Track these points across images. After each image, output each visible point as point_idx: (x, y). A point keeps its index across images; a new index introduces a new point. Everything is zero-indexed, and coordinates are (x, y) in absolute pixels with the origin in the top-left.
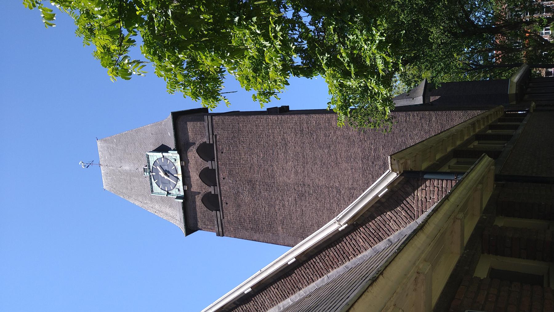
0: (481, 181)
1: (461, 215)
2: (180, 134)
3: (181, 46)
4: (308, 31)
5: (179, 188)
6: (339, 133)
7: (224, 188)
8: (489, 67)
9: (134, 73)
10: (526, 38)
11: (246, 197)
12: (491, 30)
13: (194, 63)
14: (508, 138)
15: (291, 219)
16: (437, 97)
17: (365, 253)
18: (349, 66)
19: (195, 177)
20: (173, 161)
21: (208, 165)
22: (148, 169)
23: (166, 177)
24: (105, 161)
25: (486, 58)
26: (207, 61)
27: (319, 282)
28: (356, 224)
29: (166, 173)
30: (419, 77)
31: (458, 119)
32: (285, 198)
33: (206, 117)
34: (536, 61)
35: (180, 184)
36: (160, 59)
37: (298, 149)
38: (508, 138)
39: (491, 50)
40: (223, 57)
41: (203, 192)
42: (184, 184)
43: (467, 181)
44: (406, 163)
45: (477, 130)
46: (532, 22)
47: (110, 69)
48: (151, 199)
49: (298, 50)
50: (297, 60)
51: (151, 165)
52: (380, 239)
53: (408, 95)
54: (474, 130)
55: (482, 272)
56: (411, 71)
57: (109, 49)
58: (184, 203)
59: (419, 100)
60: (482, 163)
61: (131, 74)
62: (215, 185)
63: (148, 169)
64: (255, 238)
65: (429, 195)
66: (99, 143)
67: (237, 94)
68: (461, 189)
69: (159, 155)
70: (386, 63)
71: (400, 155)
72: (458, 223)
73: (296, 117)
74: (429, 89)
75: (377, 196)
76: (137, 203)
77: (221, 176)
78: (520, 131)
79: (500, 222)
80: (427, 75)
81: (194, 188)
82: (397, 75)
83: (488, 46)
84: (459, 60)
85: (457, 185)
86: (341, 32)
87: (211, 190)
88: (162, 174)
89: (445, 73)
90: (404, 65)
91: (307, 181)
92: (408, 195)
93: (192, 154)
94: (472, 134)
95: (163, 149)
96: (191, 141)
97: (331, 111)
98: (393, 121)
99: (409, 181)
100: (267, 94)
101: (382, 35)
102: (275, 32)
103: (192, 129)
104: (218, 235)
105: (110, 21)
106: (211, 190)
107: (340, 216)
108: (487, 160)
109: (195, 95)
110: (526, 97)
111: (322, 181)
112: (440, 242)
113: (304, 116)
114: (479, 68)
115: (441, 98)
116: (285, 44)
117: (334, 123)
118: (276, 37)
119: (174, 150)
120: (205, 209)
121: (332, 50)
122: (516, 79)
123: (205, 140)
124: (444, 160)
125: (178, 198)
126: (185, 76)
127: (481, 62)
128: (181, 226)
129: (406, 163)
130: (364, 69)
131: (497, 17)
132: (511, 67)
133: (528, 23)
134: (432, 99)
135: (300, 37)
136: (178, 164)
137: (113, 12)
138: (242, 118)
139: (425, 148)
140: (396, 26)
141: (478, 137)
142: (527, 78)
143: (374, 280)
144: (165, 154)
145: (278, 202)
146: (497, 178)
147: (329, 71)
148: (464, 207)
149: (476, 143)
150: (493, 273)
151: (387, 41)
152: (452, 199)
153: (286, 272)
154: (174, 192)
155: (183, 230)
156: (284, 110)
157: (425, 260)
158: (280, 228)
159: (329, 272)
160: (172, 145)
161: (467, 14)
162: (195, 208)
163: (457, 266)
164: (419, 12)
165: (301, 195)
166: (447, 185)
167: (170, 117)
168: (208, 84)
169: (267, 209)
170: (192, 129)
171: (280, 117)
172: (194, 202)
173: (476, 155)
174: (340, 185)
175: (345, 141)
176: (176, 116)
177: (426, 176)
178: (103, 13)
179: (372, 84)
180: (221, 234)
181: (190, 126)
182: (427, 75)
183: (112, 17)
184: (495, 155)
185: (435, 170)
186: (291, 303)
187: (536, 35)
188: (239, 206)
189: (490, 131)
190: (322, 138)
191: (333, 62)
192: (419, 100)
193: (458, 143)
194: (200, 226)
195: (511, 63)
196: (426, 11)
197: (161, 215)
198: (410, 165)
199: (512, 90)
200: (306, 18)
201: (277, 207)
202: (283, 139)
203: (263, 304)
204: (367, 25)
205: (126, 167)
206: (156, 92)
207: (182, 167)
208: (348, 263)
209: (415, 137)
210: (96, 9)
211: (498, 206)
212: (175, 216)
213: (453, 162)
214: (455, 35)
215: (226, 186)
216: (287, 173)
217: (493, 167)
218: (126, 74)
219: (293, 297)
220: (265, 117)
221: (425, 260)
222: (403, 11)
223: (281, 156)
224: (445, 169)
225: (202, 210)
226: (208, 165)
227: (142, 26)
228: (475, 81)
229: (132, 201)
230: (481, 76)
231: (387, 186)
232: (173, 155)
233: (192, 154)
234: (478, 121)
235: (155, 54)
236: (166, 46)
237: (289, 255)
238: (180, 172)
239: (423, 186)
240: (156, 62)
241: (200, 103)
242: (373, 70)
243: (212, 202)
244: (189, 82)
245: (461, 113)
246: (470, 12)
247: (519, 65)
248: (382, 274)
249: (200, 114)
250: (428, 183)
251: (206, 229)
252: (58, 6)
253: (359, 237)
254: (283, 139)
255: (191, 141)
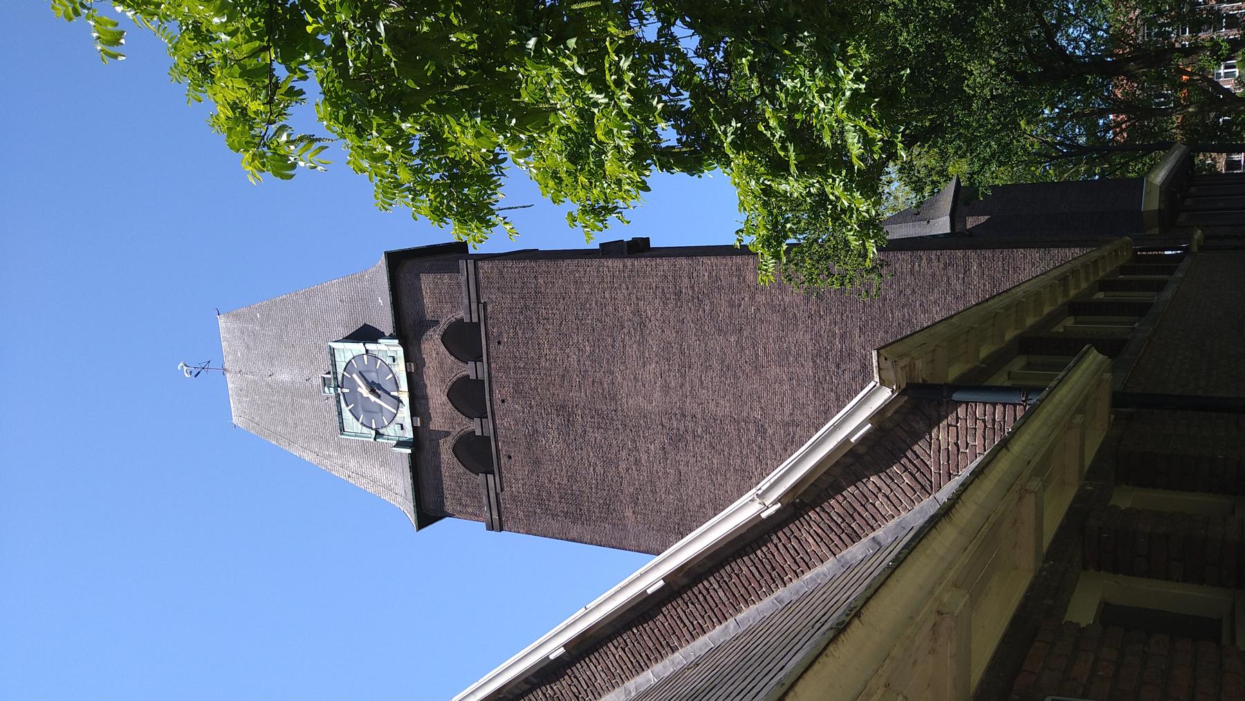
0: (1082, 406)
1: (1035, 484)
2: (405, 301)
3: (406, 104)
4: (691, 69)
5: (402, 423)
6: (761, 298)
7: (504, 423)
8: (1100, 149)
9: (301, 164)
10: (1182, 85)
11: (553, 444)
12: (1104, 67)
13: (435, 141)
14: (1141, 310)
15: (654, 492)
16: (983, 219)
17: (820, 569)
18: (784, 148)
19: (437, 397)
20: (389, 361)
21: (468, 370)
22: (334, 380)
23: (373, 398)
24: (236, 361)
25: (1091, 131)
26: (466, 137)
27: (717, 634)
28: (799, 503)
29: (374, 388)
30: (943, 173)
31: (1029, 267)
32: (641, 445)
33: (462, 263)
34: (1204, 137)
35: (405, 413)
36: (360, 132)
37: (670, 335)
38: (1141, 310)
39: (1103, 113)
40: (502, 128)
41: (457, 431)
42: (414, 413)
43: (1049, 407)
44: (911, 367)
45: (1072, 293)
46: (1195, 49)
47: (248, 156)
48: (340, 448)
49: (671, 113)
50: (668, 135)
51: (340, 370)
52: (855, 537)
53: (918, 213)
54: (1066, 292)
55: (1082, 610)
56: (924, 159)
57: (244, 111)
58: (412, 457)
59: (942, 225)
60: (1084, 366)
61: (294, 166)
62: (483, 416)
63: (334, 380)
64: (574, 534)
65: (964, 439)
66: (222, 321)
67: (532, 211)
68: (1036, 424)
69: (358, 348)
70: (867, 142)
71: (899, 348)
72: (1030, 501)
73: (665, 264)
74: (964, 200)
75: (846, 440)
76: (308, 457)
77: (497, 396)
78: (1168, 294)
79: (1124, 499)
80: (959, 168)
81: (437, 423)
82: (892, 168)
83: (1097, 103)
84: (1031, 134)
85: (1027, 416)
86: (767, 71)
87: (474, 426)
88: (364, 391)
89: (1001, 164)
90: (908, 146)
91: (691, 406)
92: (917, 437)
93: (433, 347)
94: (1060, 301)
95: (366, 334)
96: (429, 317)
97: (744, 250)
98: (884, 271)
99: (919, 407)
100: (600, 211)
101: (858, 78)
102: (619, 71)
103: (432, 289)
104: (491, 527)
105: (246, 48)
106: (474, 426)
107: (764, 484)
108: (1093, 359)
109: (439, 214)
110: (1183, 217)
111: (725, 408)
112: (988, 544)
113: (683, 262)
114: (1076, 152)
115: (992, 221)
116: (640, 99)
117: (750, 277)
118: (619, 83)
119: (391, 337)
120: (462, 469)
121: (747, 113)
122: (1159, 177)
123: (462, 314)
124: (998, 360)
125: (400, 444)
126: (416, 171)
127: (1082, 140)
128: (407, 508)
129: (911, 367)
130: (818, 156)
131: (1117, 38)
132: (1148, 150)
133: (1186, 52)
134: (971, 222)
135: (675, 82)
136: (400, 369)
137: (254, 26)
138: (543, 265)
139: (954, 333)
140: (890, 59)
141: (1075, 308)
142: (1185, 174)
143: (841, 629)
144: (370, 346)
145: (624, 454)
146: (1118, 400)
147: (739, 160)
148: (1043, 466)
149: (1069, 322)
150: (1108, 614)
151: (870, 93)
152: (1016, 447)
153: (642, 611)
154: (392, 431)
155: (412, 517)
156: (639, 247)
157: (956, 585)
158: (629, 513)
159: (738, 611)
160: (387, 326)
161: (1050, 31)
162: (438, 468)
163: (1027, 598)
164: (942, 28)
165: (677, 439)
166: (1003, 415)
167: (382, 262)
168: (467, 189)
169: (599, 470)
170: (432, 289)
171: (629, 262)
172: (437, 454)
173: (1070, 348)
174: (764, 415)
175: (776, 318)
176: (396, 261)
177: (956, 396)
178: (230, 28)
179: (836, 189)
180: (497, 525)
181: (427, 283)
182: (959, 168)
183: (251, 39)
184: (1112, 348)
185: (977, 383)
186: (653, 681)
187: (1204, 78)
188: (537, 463)
189: (1101, 295)
190: (724, 310)
191: (749, 140)
192: (942, 225)
193: (1030, 321)
194: (449, 507)
195: (1149, 142)
196: (958, 25)
197: (361, 483)
198: (922, 371)
199: (1151, 202)
200: (688, 41)
201: (623, 465)
202: (637, 312)
203: (591, 683)
204: (825, 57)
205: (284, 376)
206: (350, 207)
207: (409, 375)
208: (781, 592)
209: (932, 308)
210: (216, 20)
211: (1119, 464)
212: (394, 485)
213: (1018, 364)
214: (1022, 78)
215: (508, 417)
216: (644, 388)
217: (1108, 376)
218: (283, 167)
219: (658, 667)
220: (596, 262)
221: (956, 585)
222: (905, 24)
223: (632, 351)
224: (1001, 380)
225: (453, 471)
226: (468, 370)
227: (319, 59)
228: (1067, 182)
229: (296, 451)
230: (1080, 171)
231: (871, 419)
232: (389, 349)
233: (433, 347)
234: (1074, 272)
235: (347, 121)
236: (374, 104)
237: (649, 574)
238: (404, 386)
239: (951, 419)
240: (351, 140)
241: (450, 232)
242: (838, 158)
243: (477, 453)
244: (426, 183)
245: (1036, 254)
246: (1057, 27)
247: (1167, 146)
248: (858, 615)
249: (449, 255)
250: (961, 411)
251: (463, 514)
252: (130, 14)
253: (807, 532)
254: (637, 312)
255: (429, 317)
